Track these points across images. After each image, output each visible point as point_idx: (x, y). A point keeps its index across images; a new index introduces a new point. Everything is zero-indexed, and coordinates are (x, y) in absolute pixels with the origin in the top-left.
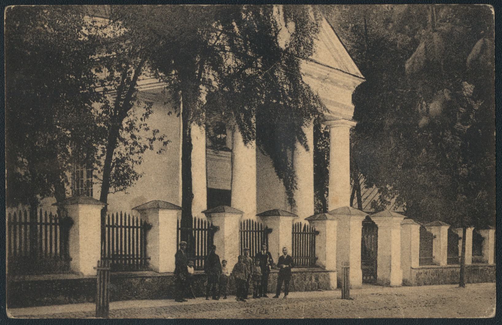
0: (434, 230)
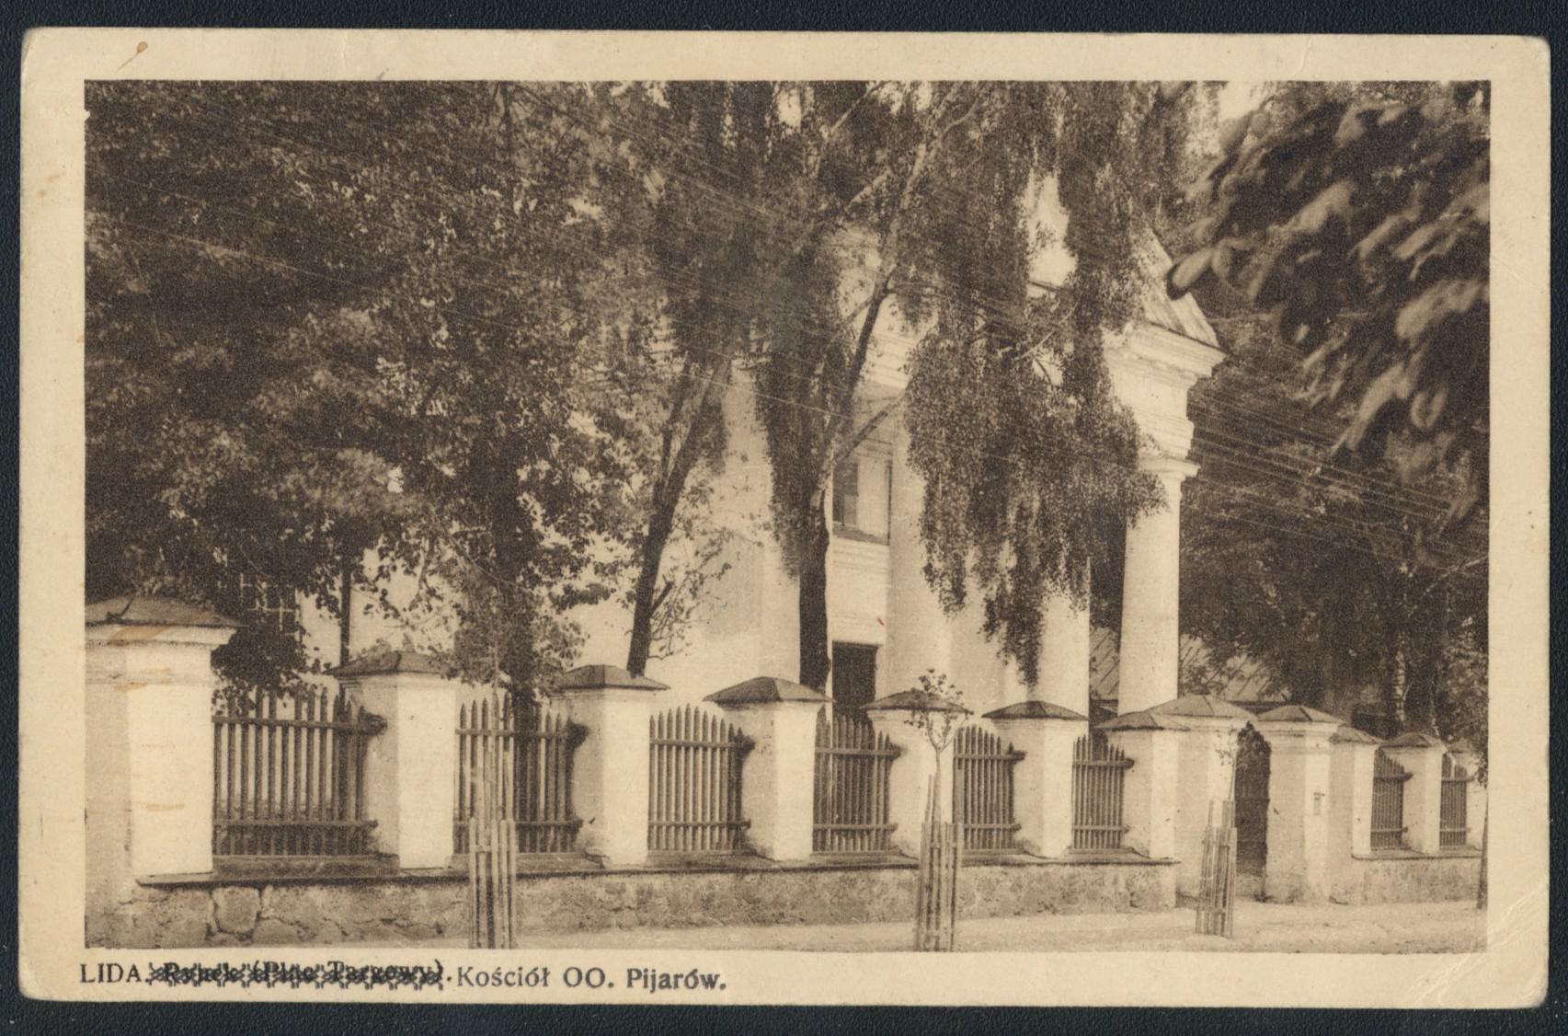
0: (1406, 759)
